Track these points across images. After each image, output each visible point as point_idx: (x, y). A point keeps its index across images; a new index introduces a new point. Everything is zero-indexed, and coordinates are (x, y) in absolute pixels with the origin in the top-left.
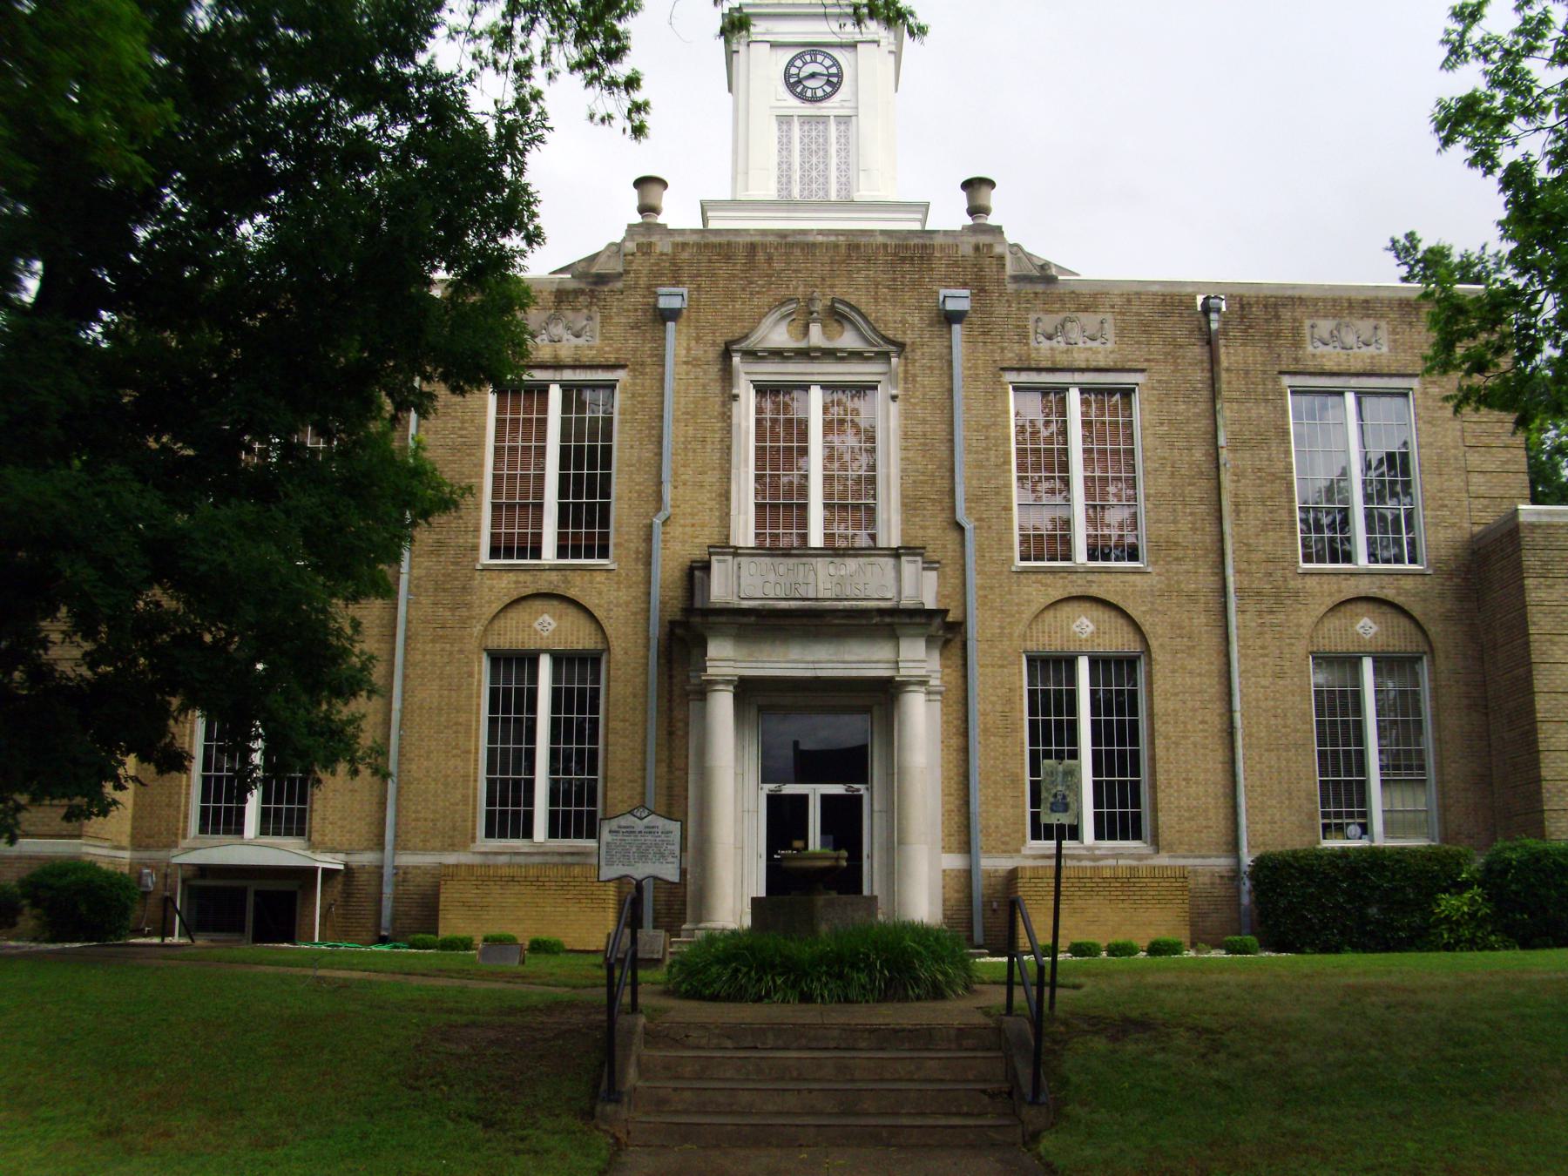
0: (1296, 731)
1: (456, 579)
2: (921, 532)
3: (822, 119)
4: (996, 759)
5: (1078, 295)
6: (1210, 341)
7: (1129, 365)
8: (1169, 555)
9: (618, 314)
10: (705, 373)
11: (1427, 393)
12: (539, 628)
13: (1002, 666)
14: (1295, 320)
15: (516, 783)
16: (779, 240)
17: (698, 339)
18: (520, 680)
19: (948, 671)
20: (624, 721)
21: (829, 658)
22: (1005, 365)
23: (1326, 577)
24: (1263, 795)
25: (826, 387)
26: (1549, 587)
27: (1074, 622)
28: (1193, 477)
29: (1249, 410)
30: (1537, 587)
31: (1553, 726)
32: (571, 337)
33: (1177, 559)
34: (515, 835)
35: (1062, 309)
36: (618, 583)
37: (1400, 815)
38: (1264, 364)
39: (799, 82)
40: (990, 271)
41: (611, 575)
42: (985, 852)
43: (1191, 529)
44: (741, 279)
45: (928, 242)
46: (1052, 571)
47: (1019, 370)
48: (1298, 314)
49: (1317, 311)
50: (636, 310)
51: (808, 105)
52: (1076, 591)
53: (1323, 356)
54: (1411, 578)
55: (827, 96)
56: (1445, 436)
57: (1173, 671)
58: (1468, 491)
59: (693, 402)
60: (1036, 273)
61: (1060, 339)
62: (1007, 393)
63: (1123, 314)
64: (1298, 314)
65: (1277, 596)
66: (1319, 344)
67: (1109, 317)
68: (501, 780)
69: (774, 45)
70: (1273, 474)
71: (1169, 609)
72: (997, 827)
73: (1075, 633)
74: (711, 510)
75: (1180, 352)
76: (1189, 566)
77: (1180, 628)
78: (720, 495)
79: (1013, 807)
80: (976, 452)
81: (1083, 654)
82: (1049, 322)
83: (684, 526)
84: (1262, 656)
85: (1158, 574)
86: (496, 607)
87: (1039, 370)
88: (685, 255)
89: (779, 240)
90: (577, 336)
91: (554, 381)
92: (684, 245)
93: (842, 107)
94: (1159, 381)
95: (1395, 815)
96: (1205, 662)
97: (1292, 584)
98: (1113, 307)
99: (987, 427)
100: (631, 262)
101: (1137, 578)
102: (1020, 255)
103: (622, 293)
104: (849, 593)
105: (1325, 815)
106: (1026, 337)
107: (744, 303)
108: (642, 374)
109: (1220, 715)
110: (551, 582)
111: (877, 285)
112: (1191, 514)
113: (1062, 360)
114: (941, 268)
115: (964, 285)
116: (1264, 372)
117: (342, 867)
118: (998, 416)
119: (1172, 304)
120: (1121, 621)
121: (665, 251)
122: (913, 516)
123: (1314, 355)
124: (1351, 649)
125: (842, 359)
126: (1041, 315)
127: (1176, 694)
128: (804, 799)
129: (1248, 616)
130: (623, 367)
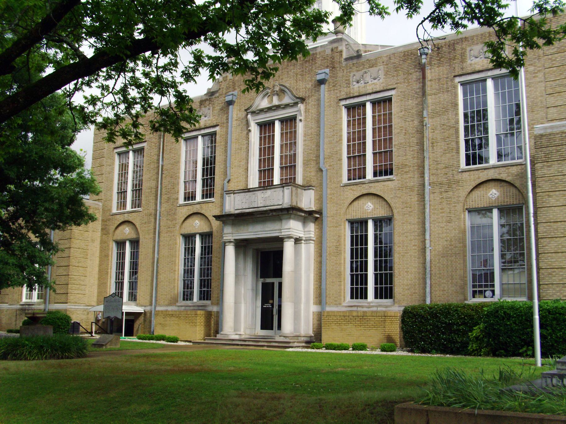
0: (456, 247)
2: (309, 174)
5: (369, 61)
6: (422, 69)
8: (402, 171)
11: (527, 71)
13: (336, 227)
14: (462, 49)
15: (361, 275)
18: (361, 232)
23: (472, 172)
26: (549, 166)
27: (365, 205)
28: (414, 133)
30: (542, 168)
31: (548, 240)
33: (406, 172)
37: (512, 286)
38: (447, 74)
40: (337, 59)
47: (346, 99)
48: (464, 46)
49: (474, 42)
50: (222, 103)
52: (365, 192)
53: (475, 64)
54: (515, 167)
56: (535, 92)
57: (403, 223)
58: (547, 118)
60: (355, 55)
62: (341, 110)
63: (387, 64)
64: (464, 46)
65: (449, 185)
66: (473, 58)
68: (380, 273)
73: (366, 210)
74: (243, 175)
75: (410, 77)
76: (411, 175)
78: (245, 169)
81: (370, 218)
82: (358, 75)
83: (234, 183)
84: (441, 213)
85: (398, 180)
87: (354, 97)
94: (401, 92)
95: (510, 285)
96: (415, 219)
97: (456, 177)
98: (383, 63)
101: (390, 182)
103: (218, 97)
104: (268, 203)
105: (474, 286)
111: (297, 74)
113: (363, 91)
114: (319, 62)
115: (327, 67)
116: (447, 78)
117: (143, 311)
119: (408, 55)
123: (471, 64)
124: (485, 206)
125: (284, 108)
126: (355, 73)
127: (404, 234)
128: (273, 283)
129: (436, 194)
130: (218, 125)
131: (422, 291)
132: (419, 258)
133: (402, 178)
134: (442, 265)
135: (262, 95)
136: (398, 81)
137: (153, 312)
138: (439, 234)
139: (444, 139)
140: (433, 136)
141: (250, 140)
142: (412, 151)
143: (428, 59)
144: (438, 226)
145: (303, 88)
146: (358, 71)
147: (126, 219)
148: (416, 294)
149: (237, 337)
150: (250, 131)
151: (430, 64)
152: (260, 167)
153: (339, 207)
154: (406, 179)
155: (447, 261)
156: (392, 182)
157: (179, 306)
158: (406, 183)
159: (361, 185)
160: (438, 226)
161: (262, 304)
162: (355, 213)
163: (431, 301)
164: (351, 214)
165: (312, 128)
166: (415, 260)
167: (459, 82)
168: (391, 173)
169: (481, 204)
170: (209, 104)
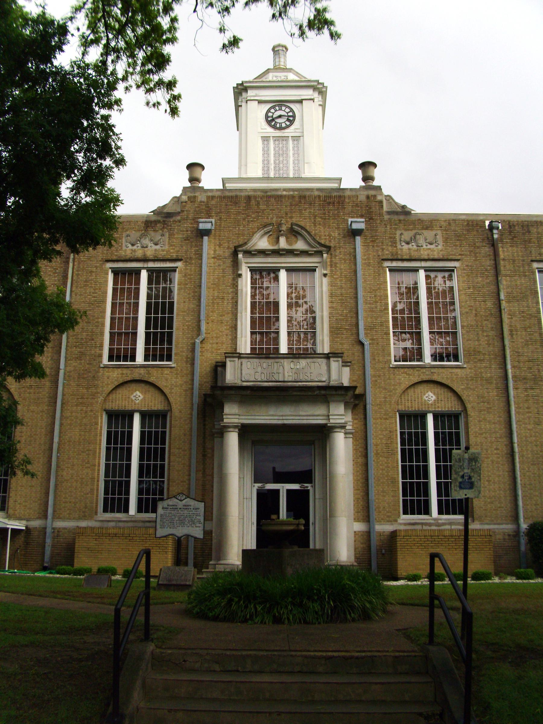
4: (382, 470)
5: (422, 221)
7: (450, 257)
12: (134, 398)
13: (386, 419)
15: (120, 483)
16: (263, 194)
19: (356, 421)
20: (178, 449)
21: (290, 413)
22: (384, 258)
24: (531, 489)
25: (289, 270)
27: (424, 394)
28: (487, 316)
32: (153, 245)
33: (480, 360)
35: (414, 228)
36: (177, 374)
38: (523, 257)
39: (273, 120)
41: (173, 370)
43: (487, 344)
44: (243, 214)
45: (342, 194)
47: (392, 260)
50: (187, 231)
51: (277, 131)
52: (425, 378)
55: (287, 127)
57: (480, 421)
59: (217, 278)
61: (413, 244)
63: (445, 230)
67: (439, 232)
68: (112, 481)
69: (260, 102)
70: (530, 315)
73: (425, 400)
74: (227, 335)
77: (483, 397)
78: (232, 327)
80: (370, 304)
81: (430, 412)
82: (407, 235)
85: (470, 369)
86: (110, 387)
87: (403, 260)
88: (213, 202)
89: (263, 194)
90: (156, 244)
91: (144, 268)
93: (295, 132)
94: (467, 266)
98: (441, 227)
100: (185, 206)
101: (459, 370)
104: (301, 378)
106: (395, 243)
110: (140, 374)
113: (415, 255)
115: (362, 216)
116: (523, 260)
117: (24, 528)
118: (381, 284)
121: (203, 200)
122: (337, 338)
126: (403, 232)
127: (482, 434)
130: (180, 260)
131: (509, 505)
133: (475, 367)
134: (533, 474)
135: (262, 232)
136: (463, 253)
137: (49, 530)
139: (525, 329)
141: (239, 288)
142: (487, 336)
144: (525, 428)
145: (325, 236)
146: (406, 230)
148: (503, 509)
153: (388, 393)
154: (480, 368)
155: (539, 469)
156: (463, 370)
159: (419, 369)
160: (525, 428)
162: (410, 404)
164: (405, 405)
165: (341, 287)
167: (110, 268)
168: (169, 359)
169: (155, 406)
170: (164, 228)
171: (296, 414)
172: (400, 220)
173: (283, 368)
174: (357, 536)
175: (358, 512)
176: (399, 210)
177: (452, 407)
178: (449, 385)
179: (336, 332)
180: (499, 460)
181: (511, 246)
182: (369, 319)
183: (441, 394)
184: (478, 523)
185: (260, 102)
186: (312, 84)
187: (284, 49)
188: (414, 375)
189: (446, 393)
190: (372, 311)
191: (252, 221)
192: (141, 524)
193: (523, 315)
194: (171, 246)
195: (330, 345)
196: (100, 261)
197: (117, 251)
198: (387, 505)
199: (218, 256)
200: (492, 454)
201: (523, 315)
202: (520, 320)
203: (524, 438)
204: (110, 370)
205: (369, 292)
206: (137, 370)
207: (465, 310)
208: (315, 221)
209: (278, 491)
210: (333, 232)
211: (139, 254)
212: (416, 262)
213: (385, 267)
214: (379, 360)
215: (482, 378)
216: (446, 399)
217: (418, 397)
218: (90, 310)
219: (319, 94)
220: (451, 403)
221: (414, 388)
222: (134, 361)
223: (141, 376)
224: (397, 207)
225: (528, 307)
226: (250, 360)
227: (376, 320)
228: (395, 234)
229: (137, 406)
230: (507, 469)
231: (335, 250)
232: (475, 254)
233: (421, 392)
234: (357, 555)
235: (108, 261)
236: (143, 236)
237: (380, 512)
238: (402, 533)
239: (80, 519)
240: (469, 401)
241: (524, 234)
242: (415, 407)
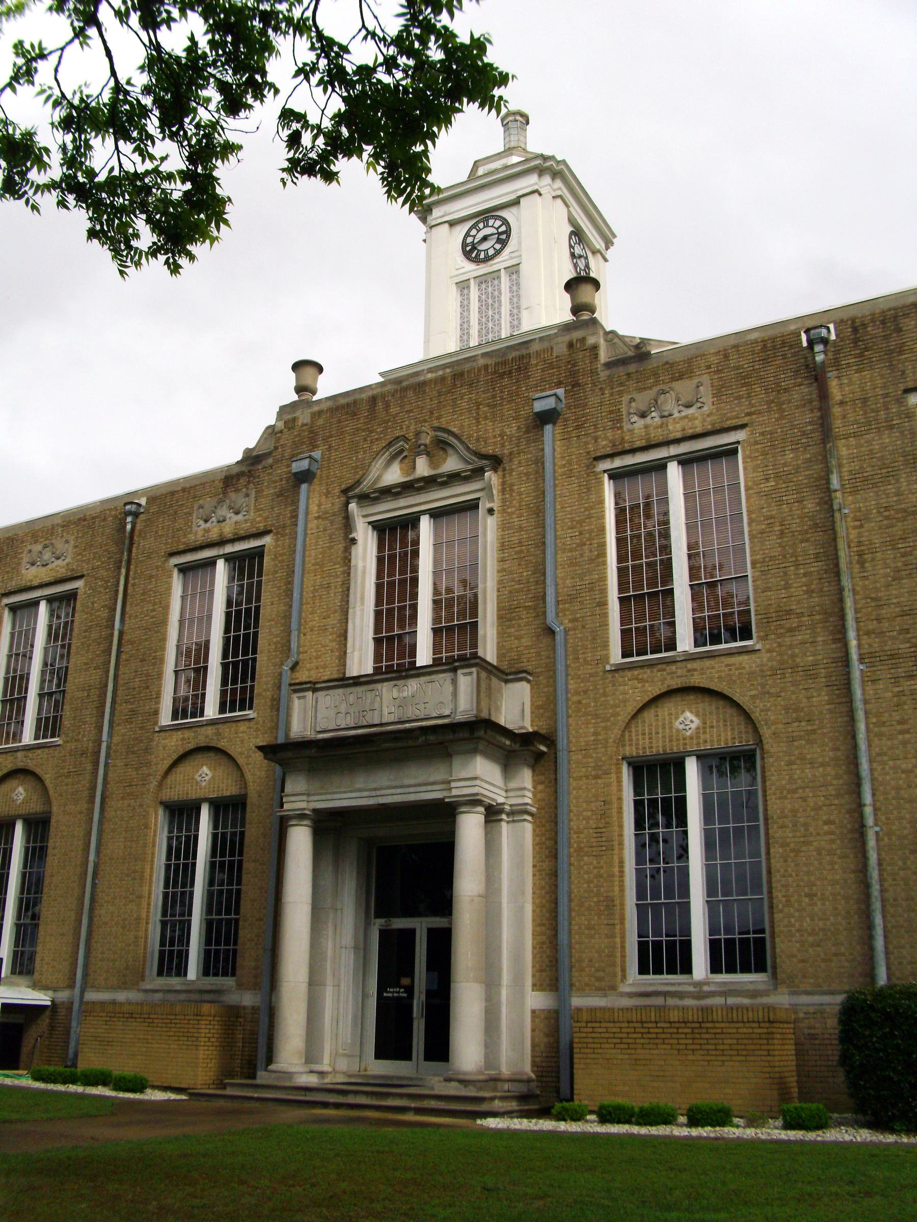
1: (141, 741)
3: (493, 275)
4: (589, 882)
5: (672, 365)
7: (729, 423)
9: (268, 487)
10: (332, 523)
12: (199, 779)
13: (596, 777)
15: (229, 921)
16: (395, 387)
17: (327, 494)
19: (540, 787)
20: (255, 861)
21: (389, 783)
22: (599, 454)
25: (436, 514)
27: (677, 718)
28: (806, 532)
29: (869, 442)
32: (232, 515)
33: (791, 630)
34: (672, 971)
35: (657, 383)
36: (257, 730)
38: (884, 386)
39: (474, 248)
41: (252, 723)
42: (578, 990)
43: (806, 592)
44: (364, 430)
45: (524, 352)
46: (650, 665)
47: (612, 456)
50: (281, 480)
51: (482, 265)
52: (676, 683)
55: (498, 253)
57: (790, 763)
59: (321, 553)
61: (653, 414)
62: (601, 483)
67: (706, 379)
69: (452, 224)
70: (904, 511)
71: (783, 690)
72: (591, 961)
73: (678, 730)
74: (332, 651)
77: (796, 710)
78: (339, 636)
79: (607, 936)
80: (571, 550)
81: (690, 754)
82: (642, 400)
83: (309, 670)
84: (902, 732)
85: (769, 651)
87: (633, 451)
88: (320, 422)
89: (395, 387)
90: (237, 513)
91: (219, 557)
92: (320, 413)
93: (512, 258)
94: (762, 434)
99: (580, 523)
100: (279, 439)
101: (745, 658)
102: (616, 340)
104: (410, 713)
106: (620, 420)
107: (365, 452)
108: (283, 535)
109: (849, 812)
110: (207, 736)
111: (478, 405)
112: (805, 575)
113: (657, 435)
114: (536, 374)
116: (886, 395)
117: (49, 1003)
118: (592, 508)
120: (730, 711)
121: (305, 421)
122: (509, 627)
127: (794, 791)
129: (881, 685)
132: (844, 857)
133: (780, 645)
138: (898, 789)
140: (860, 535)
142: (805, 575)
143: (830, 354)
146: (640, 390)
147: (20, 765)
148: (843, 958)
149: (312, 1080)
150: (353, 541)
151: (836, 364)
152: (376, 632)
153: (602, 724)
154: (791, 647)
157: (146, 991)
158: (793, 656)
159: (664, 666)
161: (381, 989)
162: (647, 741)
163: (889, 978)
164: (637, 744)
165: (521, 529)
166: (832, 863)
170: (249, 482)
171: (398, 783)
172: (628, 374)
173: (381, 699)
174: (537, 1020)
175: (541, 971)
176: (630, 354)
177: (734, 738)
178: (726, 692)
179: (508, 616)
180: (834, 846)
181: (857, 371)
182: (568, 582)
183: (711, 713)
184: (785, 990)
185: (452, 224)
186: (533, 164)
187: (518, 118)
188: (652, 681)
189: (721, 711)
190: (573, 563)
191: (377, 440)
192: (196, 997)
193: (887, 513)
194: (259, 510)
195: (498, 643)
196: (163, 556)
197: (185, 536)
198: (596, 955)
199: (326, 513)
200: (818, 834)
201: (887, 513)
202: (880, 528)
203: (893, 792)
204: (167, 734)
205: (570, 528)
206: (203, 730)
207: (759, 527)
208: (478, 414)
209: (413, 932)
210: (509, 426)
211: (214, 535)
212: (658, 449)
213: (600, 473)
214: (585, 659)
215: (794, 668)
216: (721, 724)
217: (664, 724)
218: (146, 640)
219: (553, 179)
220: (733, 729)
221: (657, 707)
222: (202, 715)
223: (207, 740)
224: (626, 349)
225: (897, 494)
226: (330, 692)
227: (582, 580)
228: (620, 403)
229: (203, 791)
230: (852, 866)
231: (511, 461)
232: (780, 404)
233: (670, 714)
234: (537, 1059)
235: (172, 554)
236: (221, 502)
237: (582, 970)
238: (584, 1014)
239: (114, 988)
240: (766, 721)
241: (886, 337)
242: (658, 747)
